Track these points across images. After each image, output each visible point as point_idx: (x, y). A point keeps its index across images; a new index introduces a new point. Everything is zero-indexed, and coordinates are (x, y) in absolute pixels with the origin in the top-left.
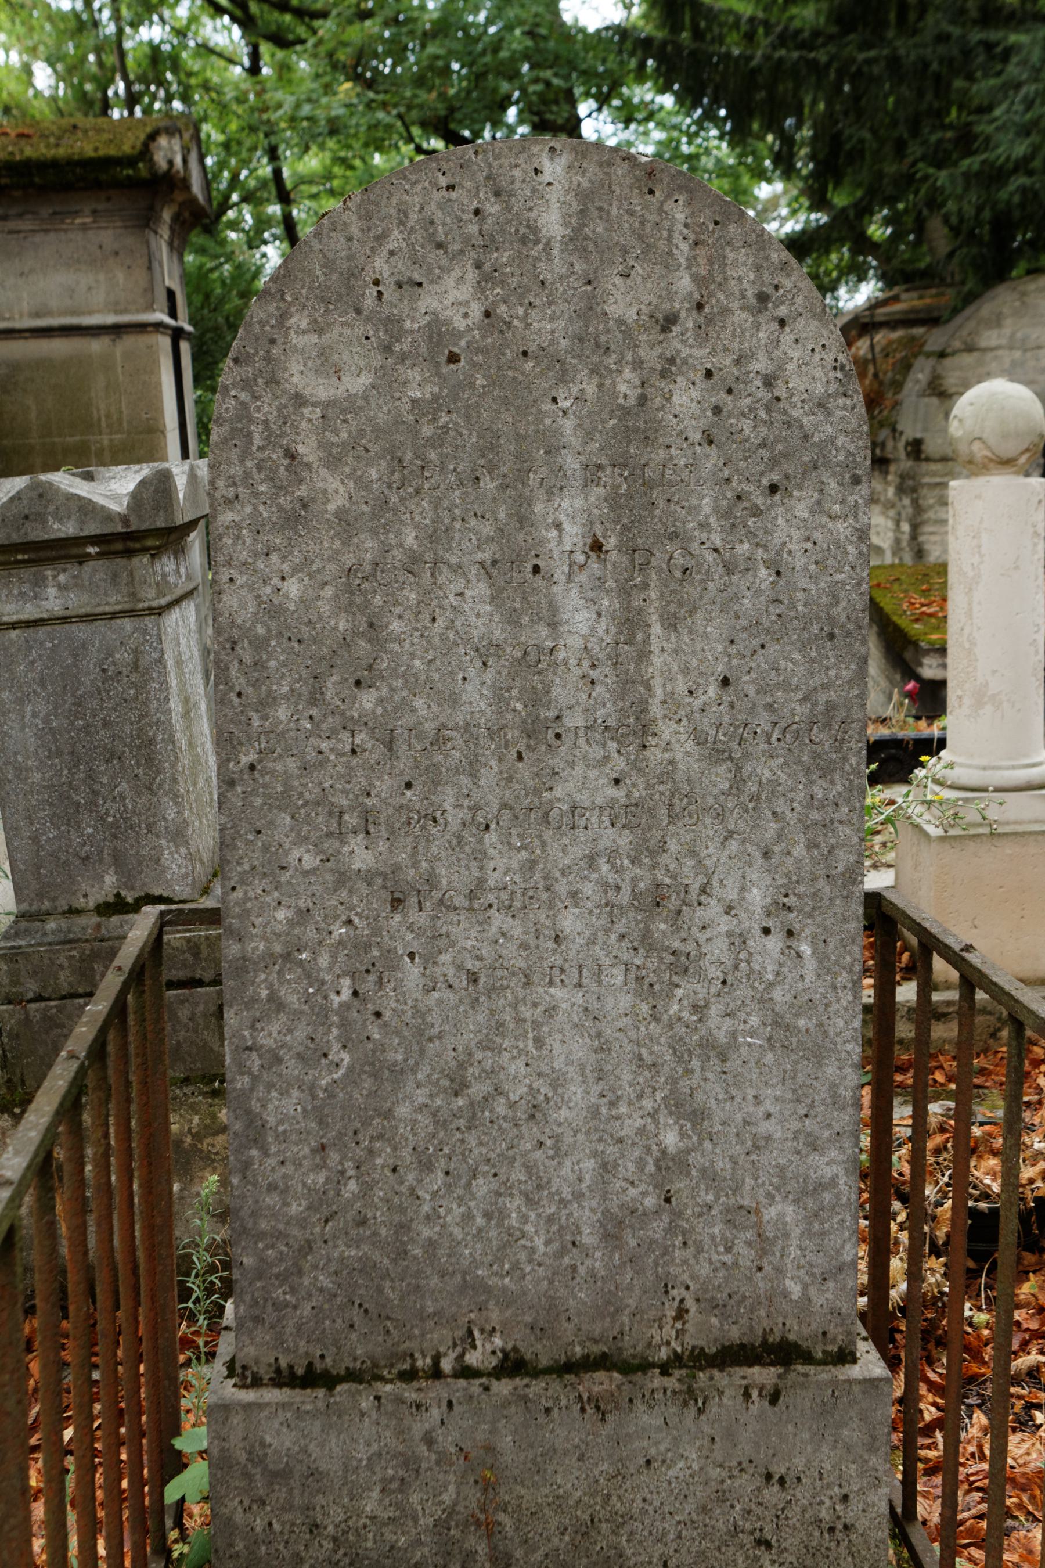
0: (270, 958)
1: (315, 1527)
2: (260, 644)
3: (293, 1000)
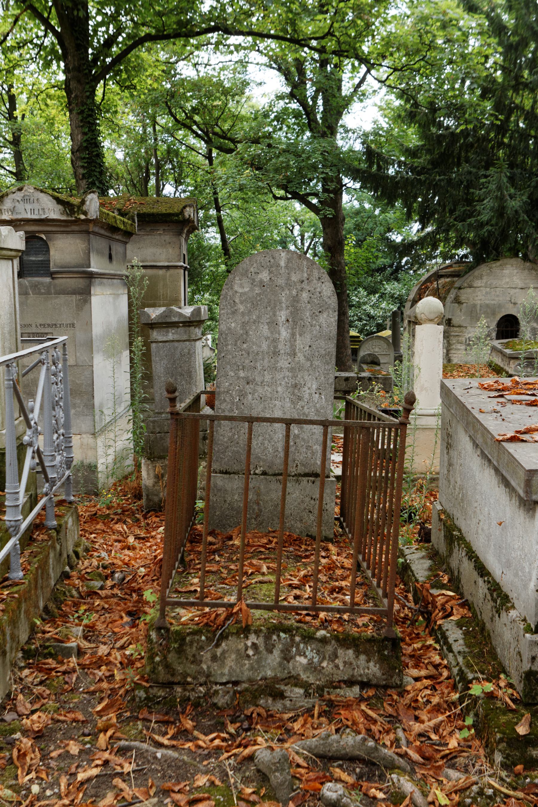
0: (224, 392)
1: (225, 501)
2: (226, 334)
3: (228, 400)
